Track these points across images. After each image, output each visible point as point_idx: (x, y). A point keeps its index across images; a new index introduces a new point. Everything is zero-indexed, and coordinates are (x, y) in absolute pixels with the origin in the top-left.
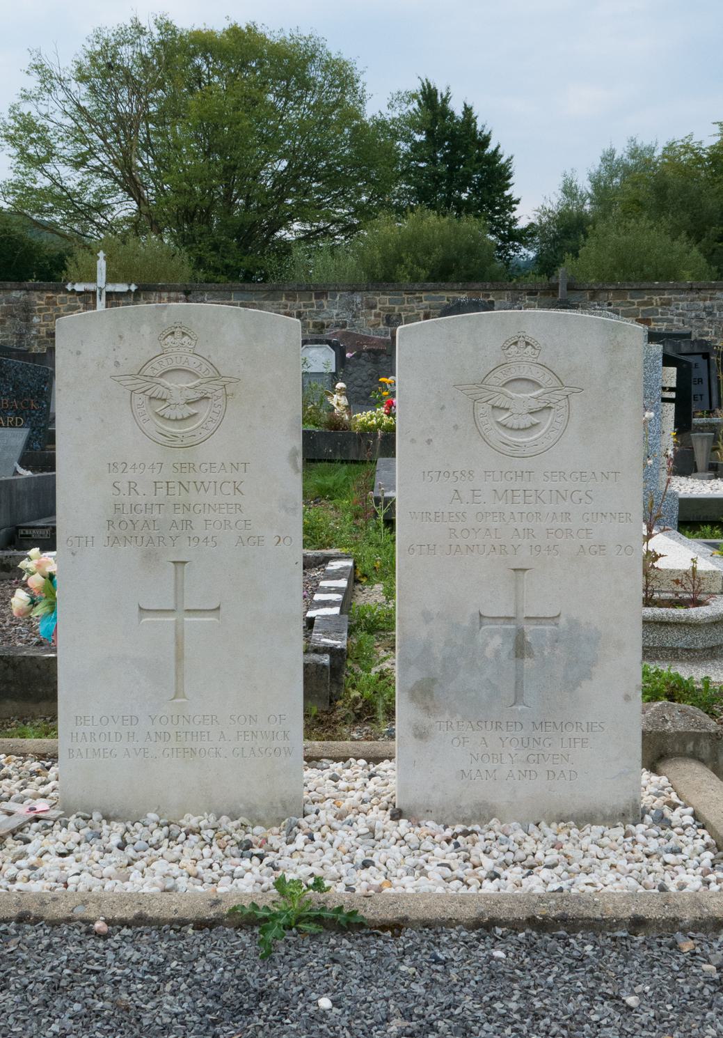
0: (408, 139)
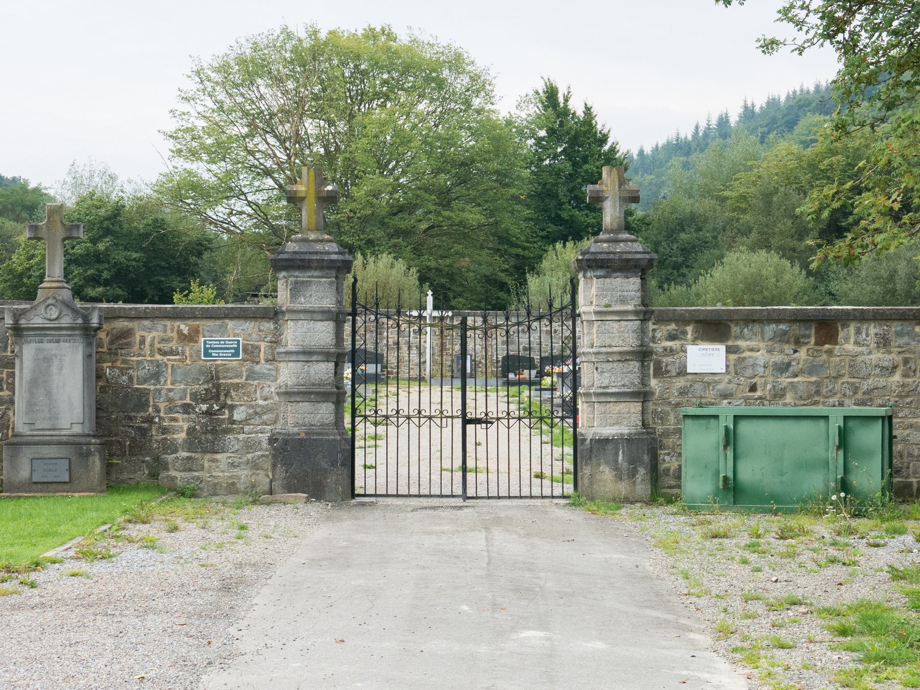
0: (533, 135)
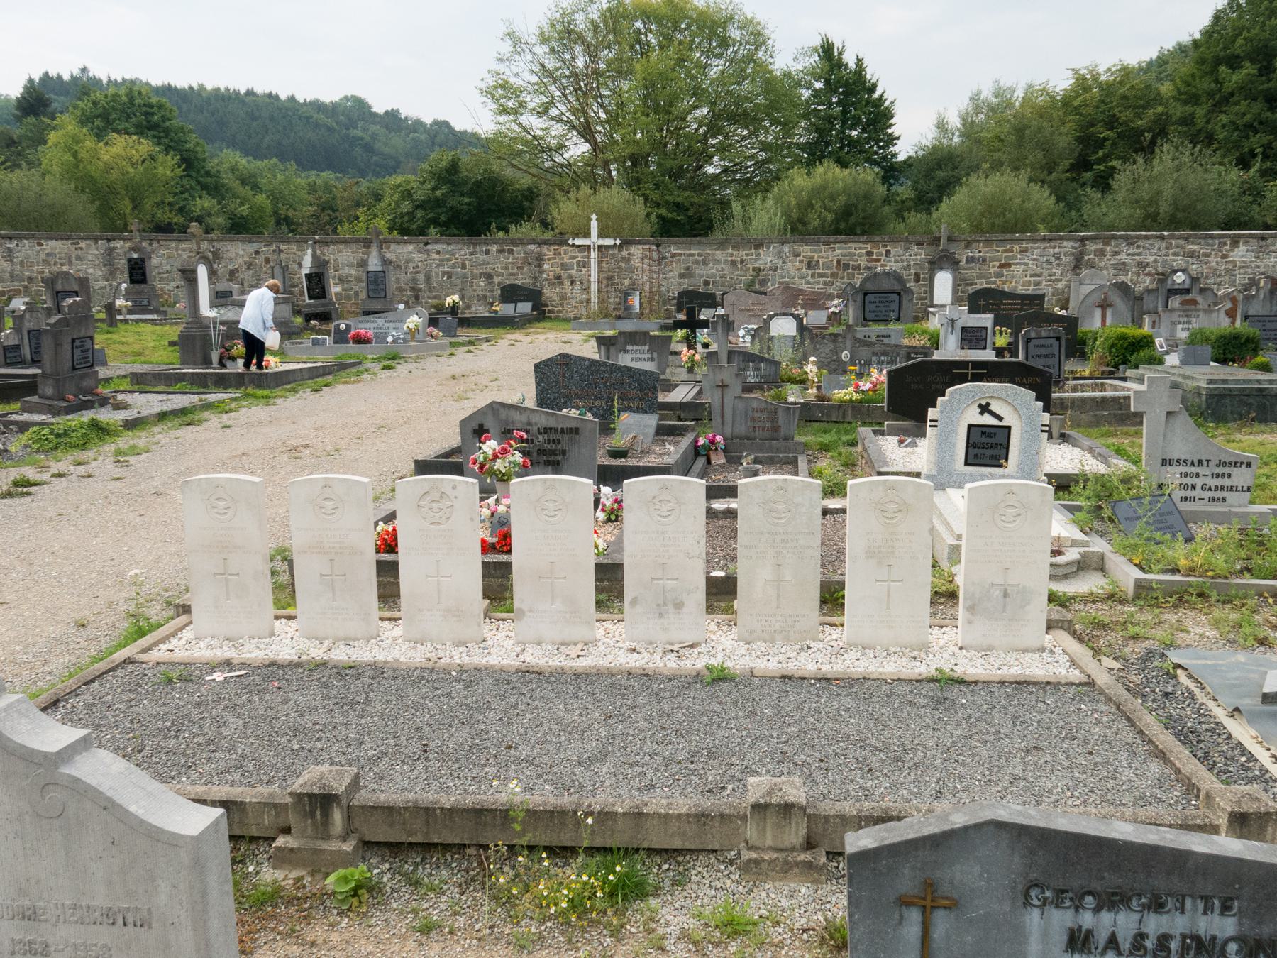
0: (809, 86)
